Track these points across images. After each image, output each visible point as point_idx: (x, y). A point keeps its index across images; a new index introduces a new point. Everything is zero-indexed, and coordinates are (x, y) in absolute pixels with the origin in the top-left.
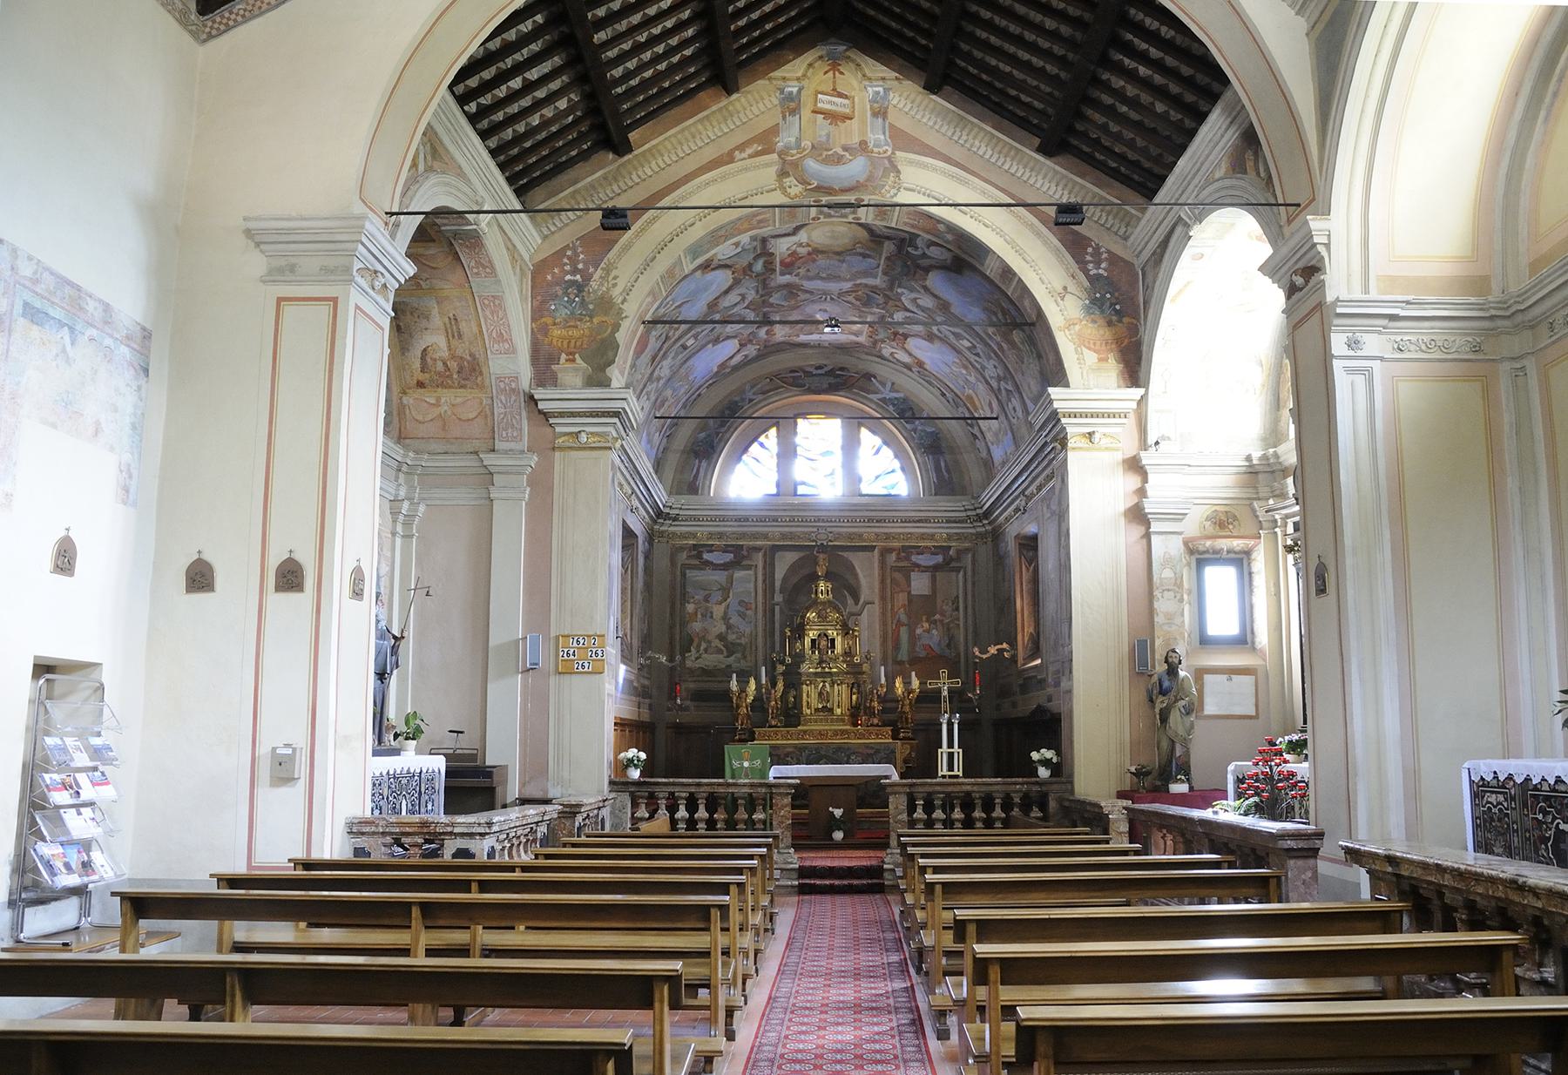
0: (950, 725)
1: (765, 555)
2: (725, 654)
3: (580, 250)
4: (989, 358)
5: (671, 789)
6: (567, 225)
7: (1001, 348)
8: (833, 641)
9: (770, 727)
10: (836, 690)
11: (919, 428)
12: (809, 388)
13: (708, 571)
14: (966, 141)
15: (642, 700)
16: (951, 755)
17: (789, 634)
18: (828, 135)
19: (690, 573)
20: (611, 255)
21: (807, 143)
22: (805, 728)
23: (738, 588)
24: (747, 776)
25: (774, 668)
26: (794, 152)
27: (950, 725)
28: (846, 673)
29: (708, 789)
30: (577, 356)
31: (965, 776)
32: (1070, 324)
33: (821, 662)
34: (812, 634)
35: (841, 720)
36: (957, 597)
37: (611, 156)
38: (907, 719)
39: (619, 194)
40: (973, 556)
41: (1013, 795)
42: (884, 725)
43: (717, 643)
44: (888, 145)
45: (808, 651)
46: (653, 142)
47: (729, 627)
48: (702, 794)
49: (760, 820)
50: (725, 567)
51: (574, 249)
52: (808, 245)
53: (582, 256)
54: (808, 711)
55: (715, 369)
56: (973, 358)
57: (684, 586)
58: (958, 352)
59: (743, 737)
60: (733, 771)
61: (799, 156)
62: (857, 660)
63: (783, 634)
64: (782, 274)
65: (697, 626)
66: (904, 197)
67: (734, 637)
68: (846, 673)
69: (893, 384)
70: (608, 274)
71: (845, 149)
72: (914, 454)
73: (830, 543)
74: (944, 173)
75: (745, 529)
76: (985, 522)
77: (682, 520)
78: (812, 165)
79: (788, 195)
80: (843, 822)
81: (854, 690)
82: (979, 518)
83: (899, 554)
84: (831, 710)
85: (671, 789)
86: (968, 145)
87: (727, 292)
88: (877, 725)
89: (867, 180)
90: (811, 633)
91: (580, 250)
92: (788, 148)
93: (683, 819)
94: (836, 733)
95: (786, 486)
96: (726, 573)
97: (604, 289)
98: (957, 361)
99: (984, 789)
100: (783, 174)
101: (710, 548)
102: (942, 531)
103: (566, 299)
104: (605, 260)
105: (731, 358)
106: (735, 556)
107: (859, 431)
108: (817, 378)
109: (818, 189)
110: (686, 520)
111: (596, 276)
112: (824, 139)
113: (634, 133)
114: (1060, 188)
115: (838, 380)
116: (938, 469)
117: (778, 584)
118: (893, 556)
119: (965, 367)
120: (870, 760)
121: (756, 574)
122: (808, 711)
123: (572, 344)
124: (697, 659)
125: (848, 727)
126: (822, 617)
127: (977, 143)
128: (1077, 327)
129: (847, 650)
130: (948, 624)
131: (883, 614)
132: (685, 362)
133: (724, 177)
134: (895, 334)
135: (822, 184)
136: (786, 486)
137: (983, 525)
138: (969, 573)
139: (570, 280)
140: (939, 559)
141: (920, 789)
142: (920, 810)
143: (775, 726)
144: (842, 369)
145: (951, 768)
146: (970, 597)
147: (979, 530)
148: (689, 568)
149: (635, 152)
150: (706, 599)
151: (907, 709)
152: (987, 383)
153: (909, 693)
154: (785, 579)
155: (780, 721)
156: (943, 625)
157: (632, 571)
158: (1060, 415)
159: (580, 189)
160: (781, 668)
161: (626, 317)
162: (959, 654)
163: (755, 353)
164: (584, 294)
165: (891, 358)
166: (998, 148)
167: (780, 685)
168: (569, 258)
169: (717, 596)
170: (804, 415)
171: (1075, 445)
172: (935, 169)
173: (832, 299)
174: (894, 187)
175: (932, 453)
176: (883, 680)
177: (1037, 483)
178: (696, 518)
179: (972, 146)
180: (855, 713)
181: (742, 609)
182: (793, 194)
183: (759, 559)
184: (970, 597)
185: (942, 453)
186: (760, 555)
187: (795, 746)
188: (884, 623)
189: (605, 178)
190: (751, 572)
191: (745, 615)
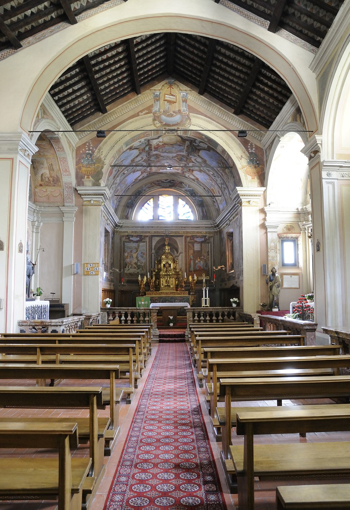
1: (149, 238)
5: (120, 311)
8: (170, 265)
9: (151, 291)
10: (171, 281)
13: (132, 243)
14: (211, 110)
16: (206, 300)
18: (169, 108)
19: (126, 244)
20: (101, 145)
21: (162, 110)
24: (143, 307)
25: (152, 273)
28: (174, 275)
31: (210, 306)
33: (166, 271)
34: (164, 263)
36: (209, 251)
37: (101, 114)
38: (193, 289)
42: (186, 291)
43: (134, 265)
47: (138, 260)
50: (137, 242)
53: (91, 145)
54: (163, 286)
55: (134, 181)
57: (124, 248)
58: (209, 175)
62: (177, 270)
63: (155, 262)
64: (154, 151)
65: (128, 260)
68: (174, 275)
69: (189, 185)
70: (100, 151)
71: (174, 112)
74: (204, 120)
76: (217, 228)
78: (163, 117)
79: (156, 127)
82: (215, 227)
83: (190, 238)
84: (169, 286)
85: (120, 311)
87: (137, 157)
88: (184, 291)
91: (91, 143)
92: (156, 112)
94: (171, 293)
97: (99, 155)
100: (154, 120)
101: (132, 236)
104: (99, 146)
106: (140, 238)
111: (96, 151)
112: (167, 109)
113: (107, 107)
115: (172, 184)
116: (203, 211)
117: (153, 247)
121: (146, 244)
122: (163, 286)
123: (88, 173)
124: (128, 270)
127: (215, 111)
128: (245, 168)
131: (186, 256)
132: (125, 178)
133: (136, 121)
134: (190, 170)
135: (166, 123)
140: (203, 239)
142: (196, 317)
143: (152, 291)
144: (173, 181)
147: (215, 230)
149: (108, 113)
150: (131, 252)
151: (193, 286)
154: (155, 246)
155: (154, 289)
158: (240, 196)
160: (154, 273)
163: (146, 175)
166: (221, 113)
167: (154, 278)
169: (135, 251)
172: (202, 119)
173: (170, 159)
174: (189, 124)
176: (186, 277)
177: (233, 216)
178: (128, 227)
181: (142, 255)
182: (157, 126)
183: (147, 239)
185: (204, 207)
187: (159, 297)
188: (186, 260)
189: (99, 120)
190: (145, 243)
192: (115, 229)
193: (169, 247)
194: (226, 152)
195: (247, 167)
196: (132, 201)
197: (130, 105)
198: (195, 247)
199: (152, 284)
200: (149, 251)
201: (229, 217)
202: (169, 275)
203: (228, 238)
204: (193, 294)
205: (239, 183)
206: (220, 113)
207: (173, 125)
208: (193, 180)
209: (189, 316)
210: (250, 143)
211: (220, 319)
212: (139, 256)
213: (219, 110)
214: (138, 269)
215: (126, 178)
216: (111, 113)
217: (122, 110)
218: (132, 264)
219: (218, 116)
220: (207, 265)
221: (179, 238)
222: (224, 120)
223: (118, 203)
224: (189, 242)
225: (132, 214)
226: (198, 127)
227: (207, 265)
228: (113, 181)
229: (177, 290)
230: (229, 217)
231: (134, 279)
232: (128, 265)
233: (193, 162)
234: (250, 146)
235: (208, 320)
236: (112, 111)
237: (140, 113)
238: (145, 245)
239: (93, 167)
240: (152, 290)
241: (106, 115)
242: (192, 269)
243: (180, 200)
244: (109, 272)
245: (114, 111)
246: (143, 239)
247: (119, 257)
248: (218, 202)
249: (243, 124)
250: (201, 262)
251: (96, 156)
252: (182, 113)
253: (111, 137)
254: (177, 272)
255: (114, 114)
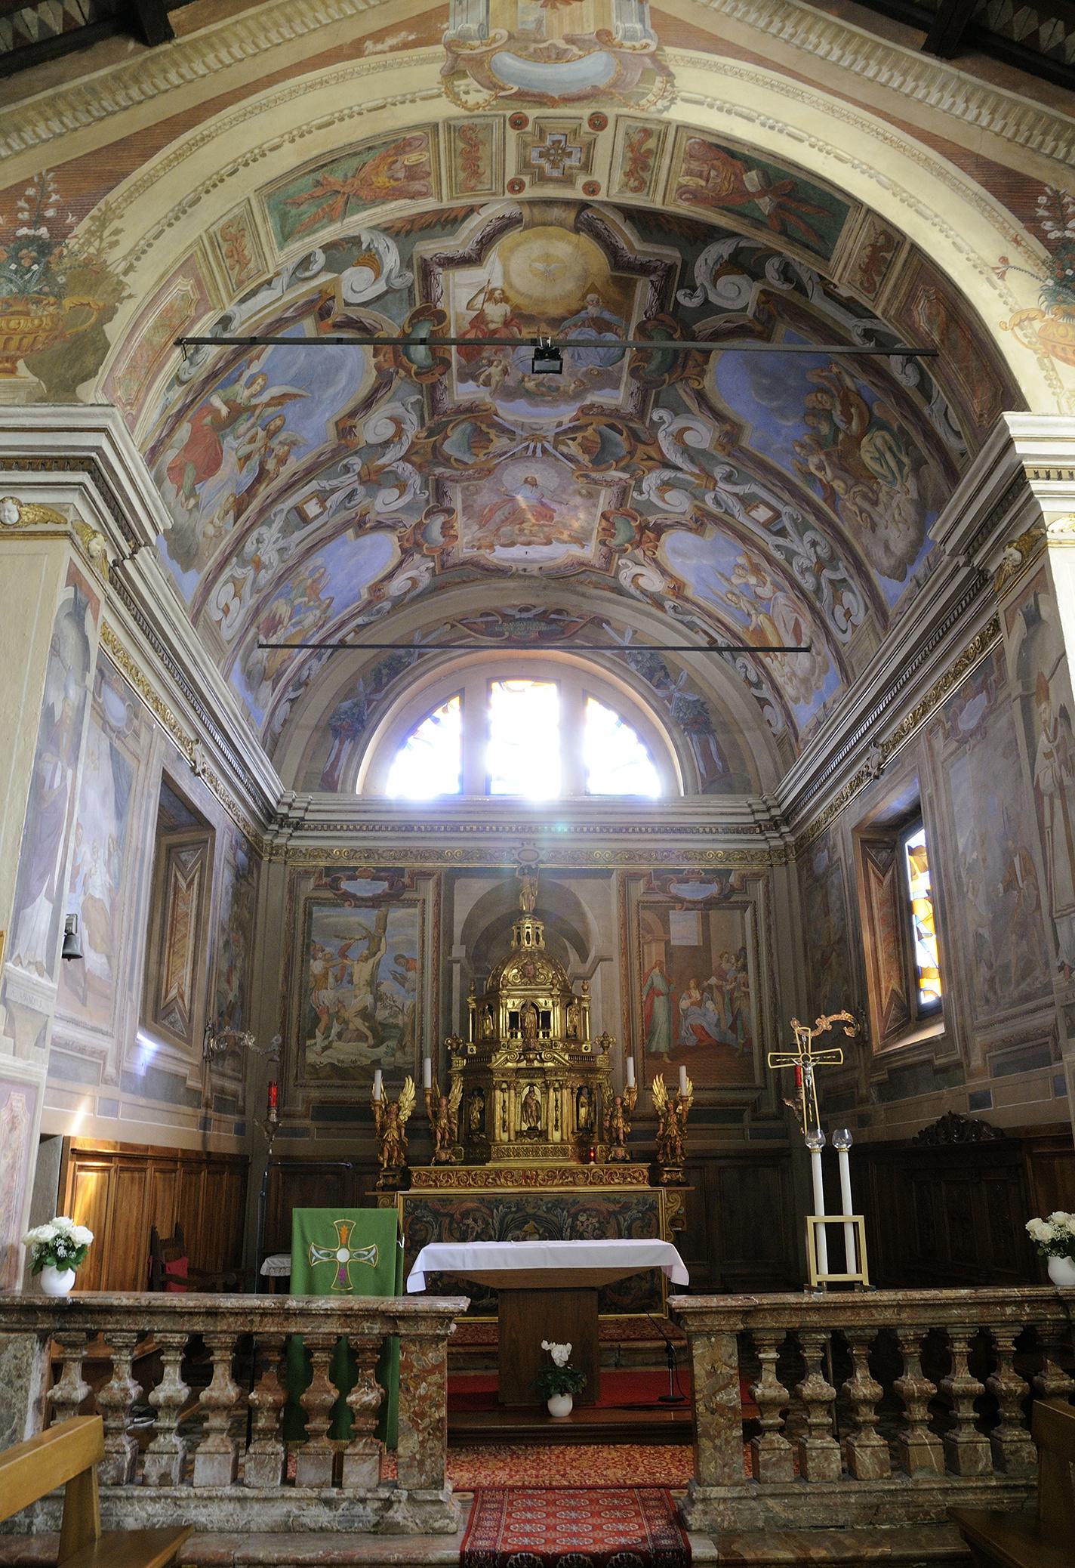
0: (830, 1158)
1: (438, 884)
2: (371, 1041)
3: (52, 186)
4: (802, 528)
5: (144, 1324)
6: (34, 146)
7: (831, 496)
8: (546, 1016)
9: (438, 1163)
10: (552, 1104)
11: (676, 695)
12: (509, 638)
13: (348, 909)
14: (792, 36)
15: (211, 1113)
16: (835, 1234)
17: (473, 1005)
18: (539, 22)
19: (318, 912)
20: (112, 196)
21: (500, 32)
22: (498, 1165)
23: (393, 937)
24: (345, 1290)
25: (449, 1064)
26: (477, 43)
27: (830, 1158)
28: (570, 1070)
29: (238, 1325)
30: (20, 364)
31: (879, 1281)
32: (1022, 319)
33: (526, 1049)
34: (512, 1004)
35: (560, 1151)
36: (744, 949)
37: (131, 45)
38: (673, 1149)
39: (140, 102)
40: (767, 885)
41: (996, 1330)
42: (633, 1160)
43: (358, 1023)
44: (651, 37)
45: (504, 1033)
46: (213, 27)
47: (378, 998)
48: (222, 1337)
49: (366, 1409)
50: (375, 902)
51: (42, 185)
52: (505, 299)
53: (54, 197)
54: (505, 1137)
55: (365, 595)
56: (770, 541)
57: (308, 933)
58: (744, 538)
59: (391, 1181)
60: (310, 1271)
61: (484, 49)
62: (587, 1048)
63: (464, 1006)
64: (463, 378)
65: (326, 996)
66: (681, 113)
67: (386, 1013)
68: (570, 1070)
69: (635, 632)
70: (103, 225)
71: (571, 40)
72: (669, 731)
73: (542, 866)
74: (755, 79)
75: (407, 844)
76: (785, 829)
77: (309, 829)
78: (509, 62)
79: (464, 105)
80: (572, 1376)
81: (583, 1099)
82: (775, 824)
83: (649, 882)
84: (543, 1134)
85: (144, 1324)
86: (796, 41)
87: (368, 403)
88: (624, 1160)
89: (614, 85)
90: (510, 1003)
91: (52, 186)
92: (462, 39)
93: (171, 1406)
94: (552, 1175)
95: (473, 780)
96: (376, 912)
97: (92, 250)
98: (741, 560)
99: (927, 1317)
100: (453, 73)
101: (353, 874)
102: (718, 847)
103: (13, 267)
104: (101, 204)
105: (390, 576)
106: (391, 886)
107: (585, 702)
108: (522, 625)
109: (521, 96)
110: (316, 829)
111: (80, 229)
112: (532, 26)
113: (177, 12)
114: (973, 106)
115: (554, 627)
116: (706, 754)
117: (458, 931)
118: (641, 886)
119: (756, 570)
120: (612, 1227)
121: (423, 913)
122: (505, 1137)
123: (14, 343)
124: (324, 1049)
125: (573, 1164)
126: (528, 976)
127: (813, 38)
128: (1037, 325)
129: (571, 1031)
130: (732, 991)
131: (627, 976)
132: (310, 551)
133: (341, 78)
134: (643, 528)
135: (526, 89)
136: (473, 780)
137: (781, 836)
138: (761, 912)
139: (27, 236)
140: (714, 889)
141: (770, 1322)
142: (769, 1376)
143: (447, 1163)
144: (559, 612)
145: (837, 1263)
146: (763, 949)
147: (773, 843)
148: (319, 904)
149: (178, 41)
150: (343, 953)
151: (674, 1131)
152: (795, 585)
153: (676, 1105)
154: (469, 924)
155: (456, 1154)
156: (722, 993)
157: (200, 885)
158: (1029, 474)
159: (67, 92)
160: (459, 1063)
161: (130, 296)
162: (749, 1043)
163: (425, 580)
164: (52, 259)
165: (632, 590)
166: (852, 47)
167: (457, 1092)
168: (29, 200)
169: (361, 948)
170: (501, 679)
171: (1061, 536)
172: (739, 74)
173: (544, 451)
174: (663, 97)
175: (696, 732)
176: (632, 1082)
177: (916, 703)
178: (329, 826)
179: (803, 42)
180: (584, 1140)
181: (400, 969)
182: (471, 103)
183: (428, 891)
184: (763, 949)
185: (712, 732)
186: (431, 884)
187: (481, 1198)
188: (628, 994)
189: (116, 77)
190: (417, 911)
191: (405, 978)
192: (267, 837)
193: (538, 924)
194: (903, 236)
195: (1049, 316)
196: (356, 705)
197: (313, 9)
198: (674, 928)
199: (443, 1122)
200: (437, 948)
201: (876, 729)
202: (543, 1071)
203: (866, 856)
204: (675, 1177)
205: (1011, 398)
206: (843, 48)
207: (567, 100)
208: (657, 601)
209: (712, 1374)
210: (1044, 194)
211: (966, 1395)
212: (383, 973)
213: (837, 35)
214: (380, 1041)
215: (317, 560)
216: (193, 44)
217: (265, 29)
218: (349, 1013)
219: (836, 64)
220: (737, 1021)
221: (591, 883)
222: (871, 80)
223: (285, 708)
224: (644, 905)
225: (354, 764)
226: (720, 109)
227: (737, 1021)
228: (232, 531)
229: (584, 1159)
230: (876, 729)
231: (353, 1095)
232: (324, 1019)
233: (667, 465)
234: (1047, 208)
235: (866, 1402)
236: (202, 32)
237: (369, 44)
238: (419, 920)
239: (44, 314)
240: (444, 1157)
241: (165, 53)
242: (661, 1043)
243: (593, 705)
244: (198, 1049)
245: (216, 33)
246: (404, 887)
247: (281, 978)
248: (789, 691)
249: (991, 101)
250: (710, 1005)
251: (72, 254)
252: (621, 46)
253: (179, 157)
254: (583, 1056)
255: (212, 46)
